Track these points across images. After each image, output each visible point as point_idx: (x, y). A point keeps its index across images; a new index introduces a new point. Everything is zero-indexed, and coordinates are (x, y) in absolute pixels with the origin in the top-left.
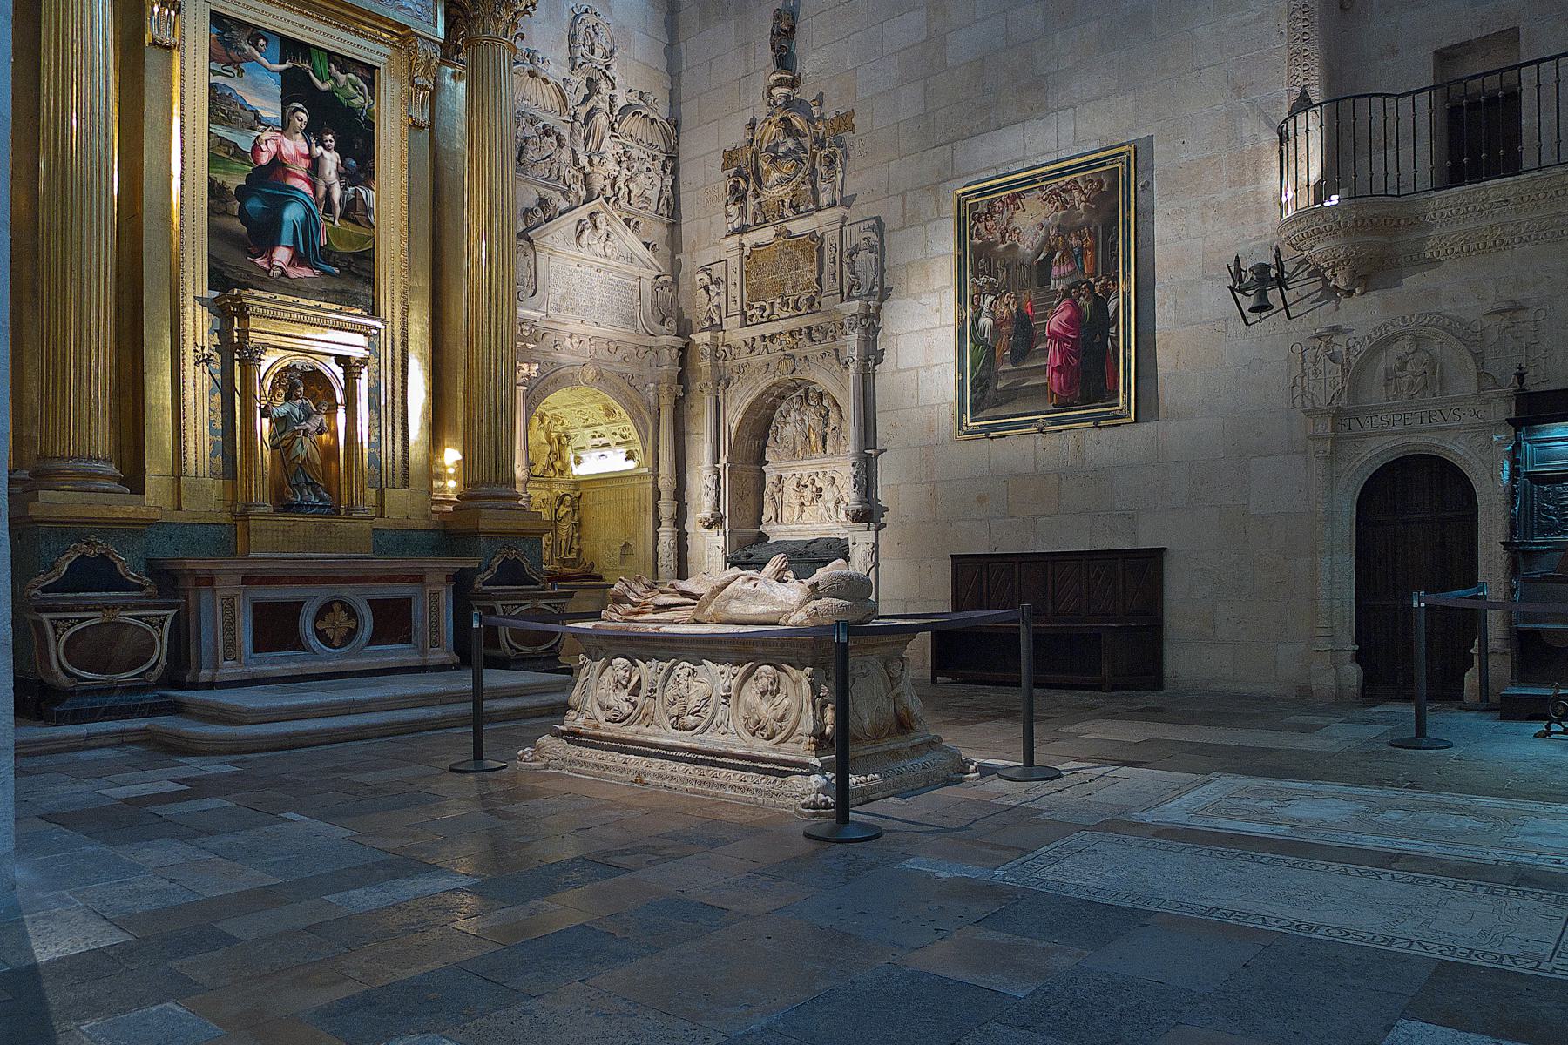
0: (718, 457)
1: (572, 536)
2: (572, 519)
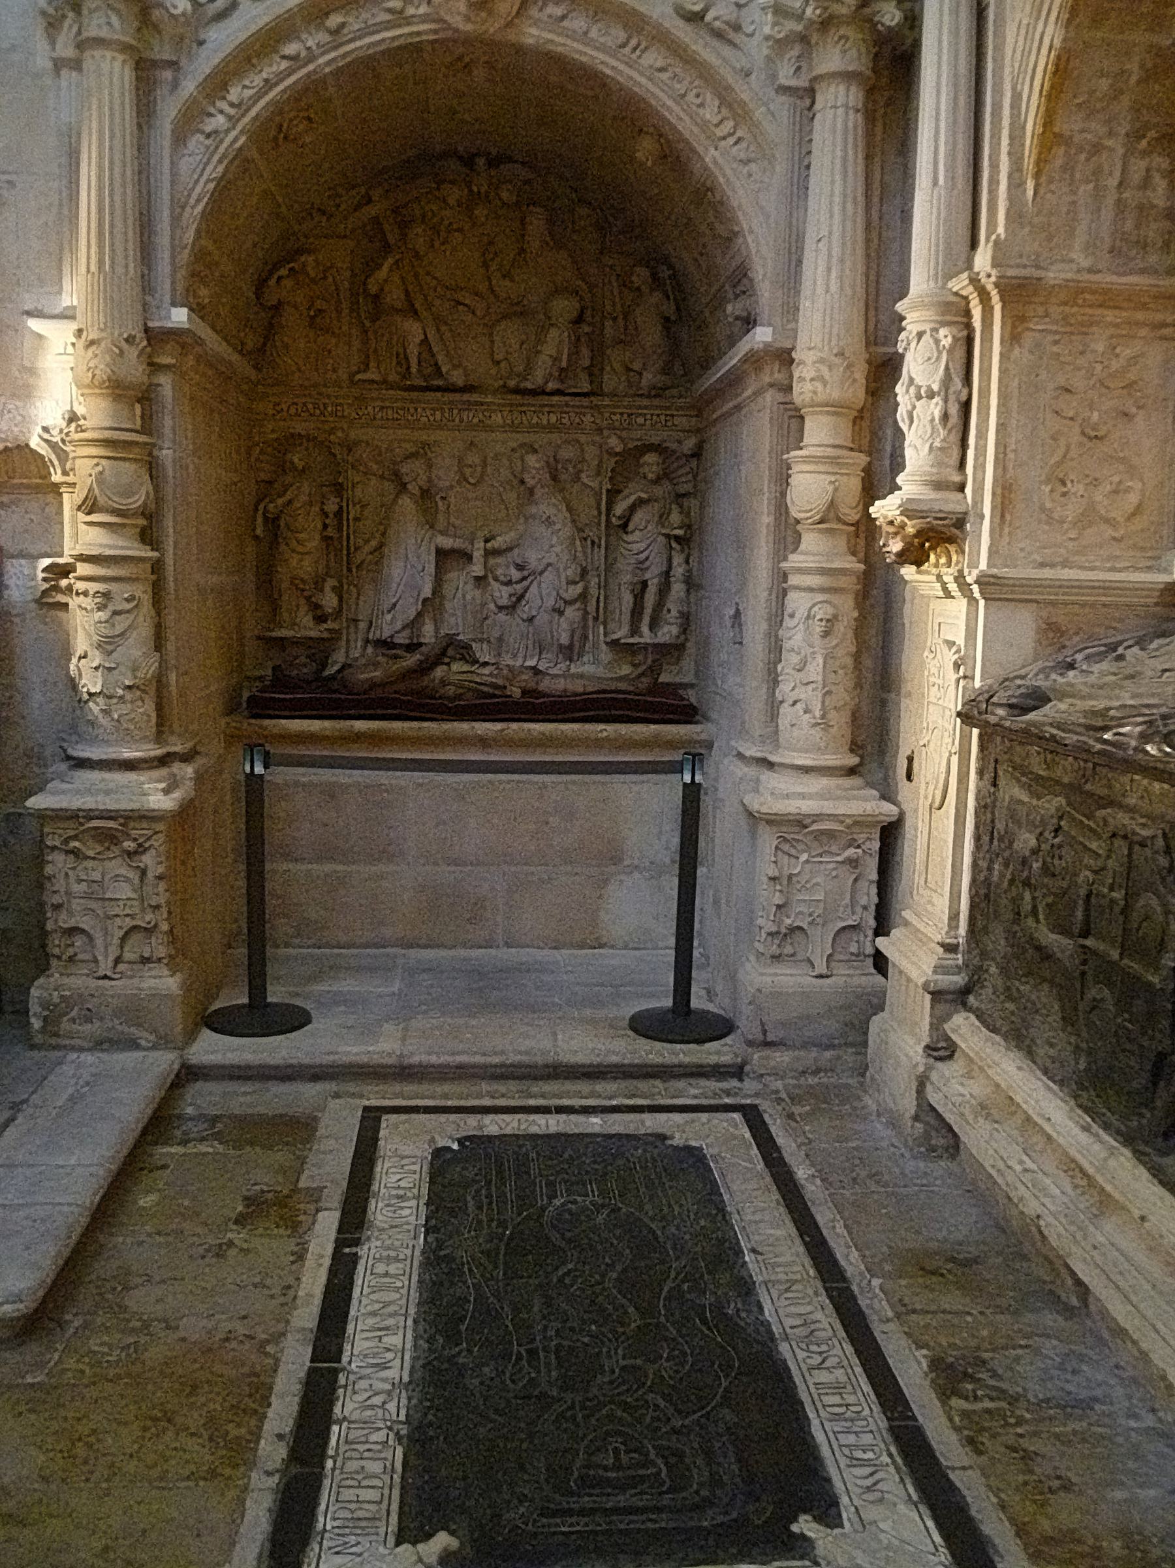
0: (974, 244)
1: (667, 574)
2: (663, 518)
